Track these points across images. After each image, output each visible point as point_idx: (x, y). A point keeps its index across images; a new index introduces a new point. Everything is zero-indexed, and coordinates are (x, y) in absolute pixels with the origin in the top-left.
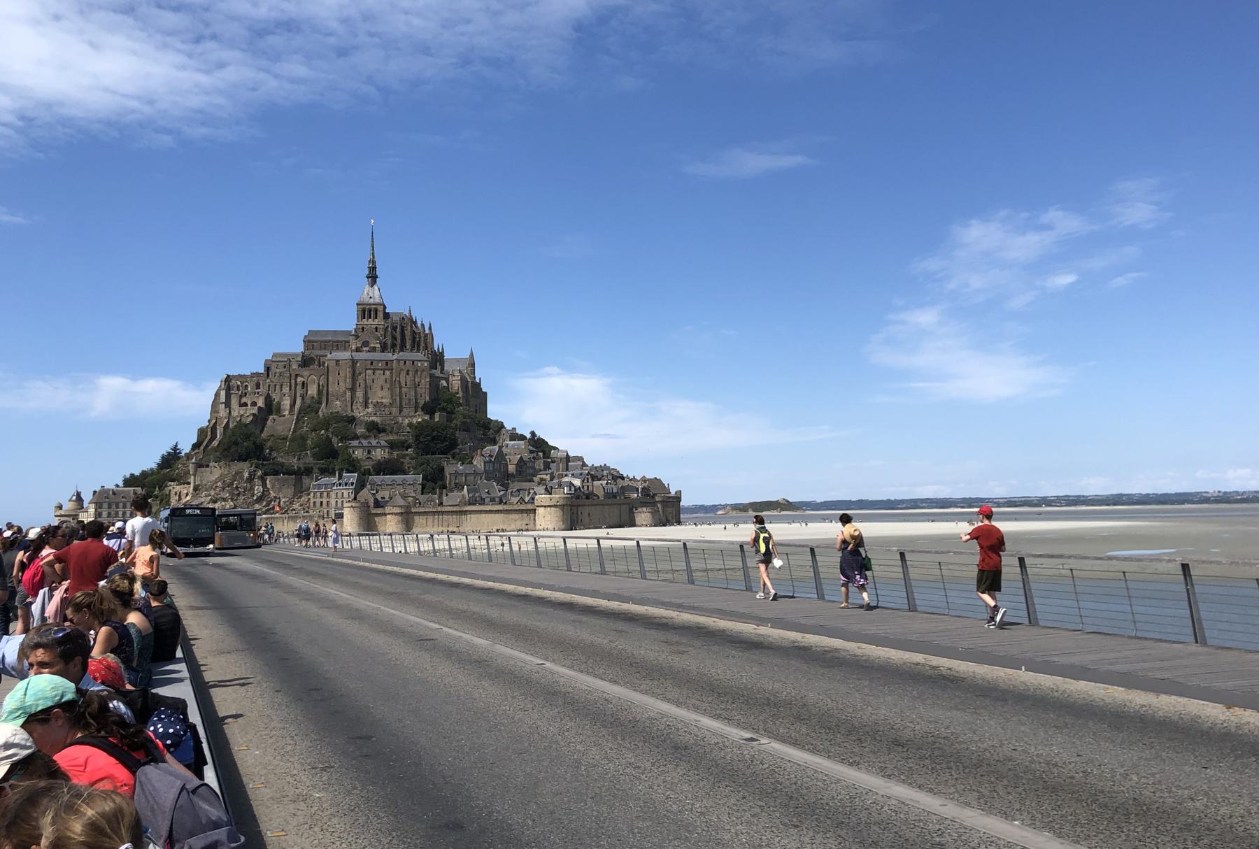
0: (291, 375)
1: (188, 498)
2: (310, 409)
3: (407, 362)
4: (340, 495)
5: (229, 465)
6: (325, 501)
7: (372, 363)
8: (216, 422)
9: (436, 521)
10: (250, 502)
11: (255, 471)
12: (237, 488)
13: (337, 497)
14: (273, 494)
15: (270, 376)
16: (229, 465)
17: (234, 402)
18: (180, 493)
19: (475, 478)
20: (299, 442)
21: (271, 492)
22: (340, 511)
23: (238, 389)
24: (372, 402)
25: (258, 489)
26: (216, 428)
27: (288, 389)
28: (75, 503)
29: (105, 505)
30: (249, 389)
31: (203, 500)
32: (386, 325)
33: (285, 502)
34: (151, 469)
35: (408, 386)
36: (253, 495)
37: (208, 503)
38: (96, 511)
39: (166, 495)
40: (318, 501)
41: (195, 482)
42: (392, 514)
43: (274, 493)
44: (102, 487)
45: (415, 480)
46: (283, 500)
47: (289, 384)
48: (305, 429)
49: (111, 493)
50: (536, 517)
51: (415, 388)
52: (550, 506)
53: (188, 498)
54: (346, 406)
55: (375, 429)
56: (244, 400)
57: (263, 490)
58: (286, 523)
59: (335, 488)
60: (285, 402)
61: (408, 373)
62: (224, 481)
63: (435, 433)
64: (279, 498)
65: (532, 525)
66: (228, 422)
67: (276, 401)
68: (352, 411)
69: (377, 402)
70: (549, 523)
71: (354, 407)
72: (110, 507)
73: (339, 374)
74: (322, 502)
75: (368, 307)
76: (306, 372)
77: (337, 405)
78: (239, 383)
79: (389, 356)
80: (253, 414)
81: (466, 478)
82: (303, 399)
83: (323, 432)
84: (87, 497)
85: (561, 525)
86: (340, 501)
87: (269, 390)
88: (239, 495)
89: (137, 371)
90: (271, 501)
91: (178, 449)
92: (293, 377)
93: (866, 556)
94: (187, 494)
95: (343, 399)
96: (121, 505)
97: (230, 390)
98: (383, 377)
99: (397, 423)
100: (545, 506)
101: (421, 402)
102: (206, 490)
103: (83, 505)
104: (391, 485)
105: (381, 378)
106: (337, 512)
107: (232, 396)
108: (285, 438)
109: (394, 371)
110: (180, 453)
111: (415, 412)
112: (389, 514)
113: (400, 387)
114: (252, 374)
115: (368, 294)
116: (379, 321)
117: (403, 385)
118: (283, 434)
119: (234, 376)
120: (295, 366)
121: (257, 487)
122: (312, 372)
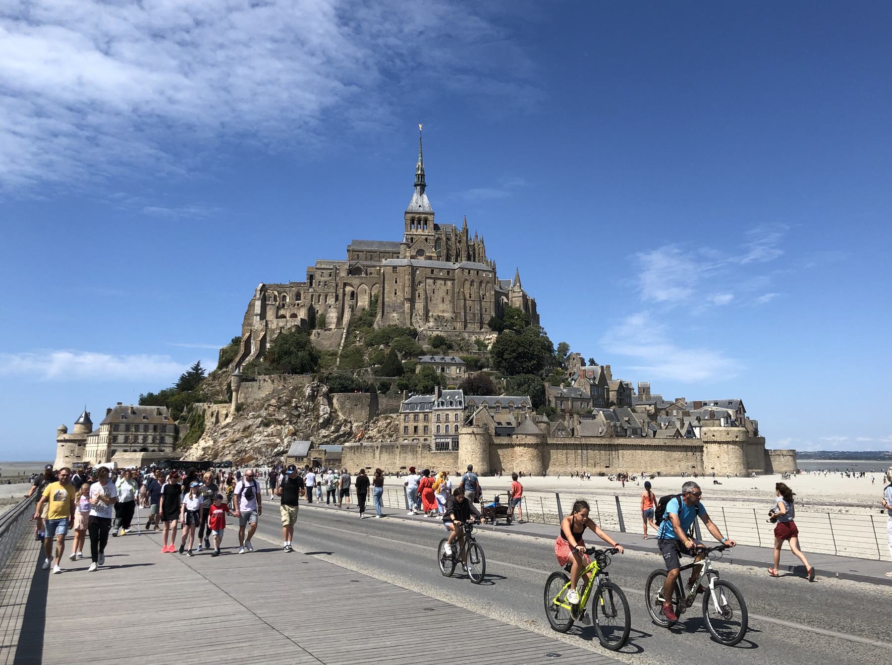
0: (337, 286)
1: (229, 420)
2: (362, 321)
3: (471, 272)
4: (443, 418)
5: (285, 379)
6: (421, 425)
7: (432, 272)
8: (250, 335)
9: (579, 457)
10: (314, 427)
11: (318, 386)
12: (296, 407)
13: (438, 420)
14: (341, 417)
15: (314, 285)
16: (285, 379)
17: (270, 315)
18: (218, 413)
19: (581, 403)
20: (353, 358)
21: (340, 414)
22: (443, 440)
23: (275, 300)
24: (432, 316)
25: (324, 410)
26: (250, 343)
27: (334, 300)
28: (83, 426)
29: (122, 427)
30: (288, 300)
31: (250, 423)
32: (436, 236)
33: (358, 427)
34: (171, 390)
35: (471, 299)
36: (318, 417)
37: (258, 427)
38: (110, 434)
39: (199, 416)
40: (411, 425)
41: (237, 400)
42: (524, 445)
43: (344, 414)
44: (119, 403)
45: (524, 402)
46: (355, 424)
47: (334, 294)
48: (358, 344)
49: (130, 411)
50: (704, 458)
51: (480, 301)
52: (728, 443)
53: (229, 420)
54: (405, 318)
55: (439, 344)
56: (282, 312)
57: (331, 411)
58: (377, 455)
59: (436, 408)
60: (331, 315)
61: (472, 285)
62: (279, 398)
63: (520, 350)
64: (350, 422)
65: (699, 468)
66: (265, 336)
67: (320, 313)
68: (411, 324)
69: (438, 316)
70: (726, 465)
71: (413, 320)
72: (128, 429)
73: (396, 282)
74: (416, 428)
75: (417, 216)
76: (355, 281)
77: (394, 318)
78: (276, 293)
79: (450, 265)
80: (297, 325)
81: (572, 404)
82: (353, 311)
83: (382, 346)
84: (98, 418)
85: (741, 469)
86: (443, 426)
87: (312, 301)
88: (299, 416)
89: (79, 347)
90: (340, 426)
91: (201, 369)
92: (341, 285)
94: (227, 416)
96: (142, 427)
97: (265, 301)
99: (463, 339)
100: (719, 443)
101: (487, 319)
102: (254, 410)
103: (91, 429)
104: (494, 407)
105: (442, 288)
106: (438, 441)
107: (268, 308)
108: (334, 354)
109: (456, 281)
110: (202, 373)
111: (481, 328)
112: (520, 445)
113: (465, 300)
114: (291, 283)
116: (429, 231)
117: (467, 296)
118: (331, 349)
119: (270, 286)
120: (343, 274)
121: (322, 407)
122: (364, 281)
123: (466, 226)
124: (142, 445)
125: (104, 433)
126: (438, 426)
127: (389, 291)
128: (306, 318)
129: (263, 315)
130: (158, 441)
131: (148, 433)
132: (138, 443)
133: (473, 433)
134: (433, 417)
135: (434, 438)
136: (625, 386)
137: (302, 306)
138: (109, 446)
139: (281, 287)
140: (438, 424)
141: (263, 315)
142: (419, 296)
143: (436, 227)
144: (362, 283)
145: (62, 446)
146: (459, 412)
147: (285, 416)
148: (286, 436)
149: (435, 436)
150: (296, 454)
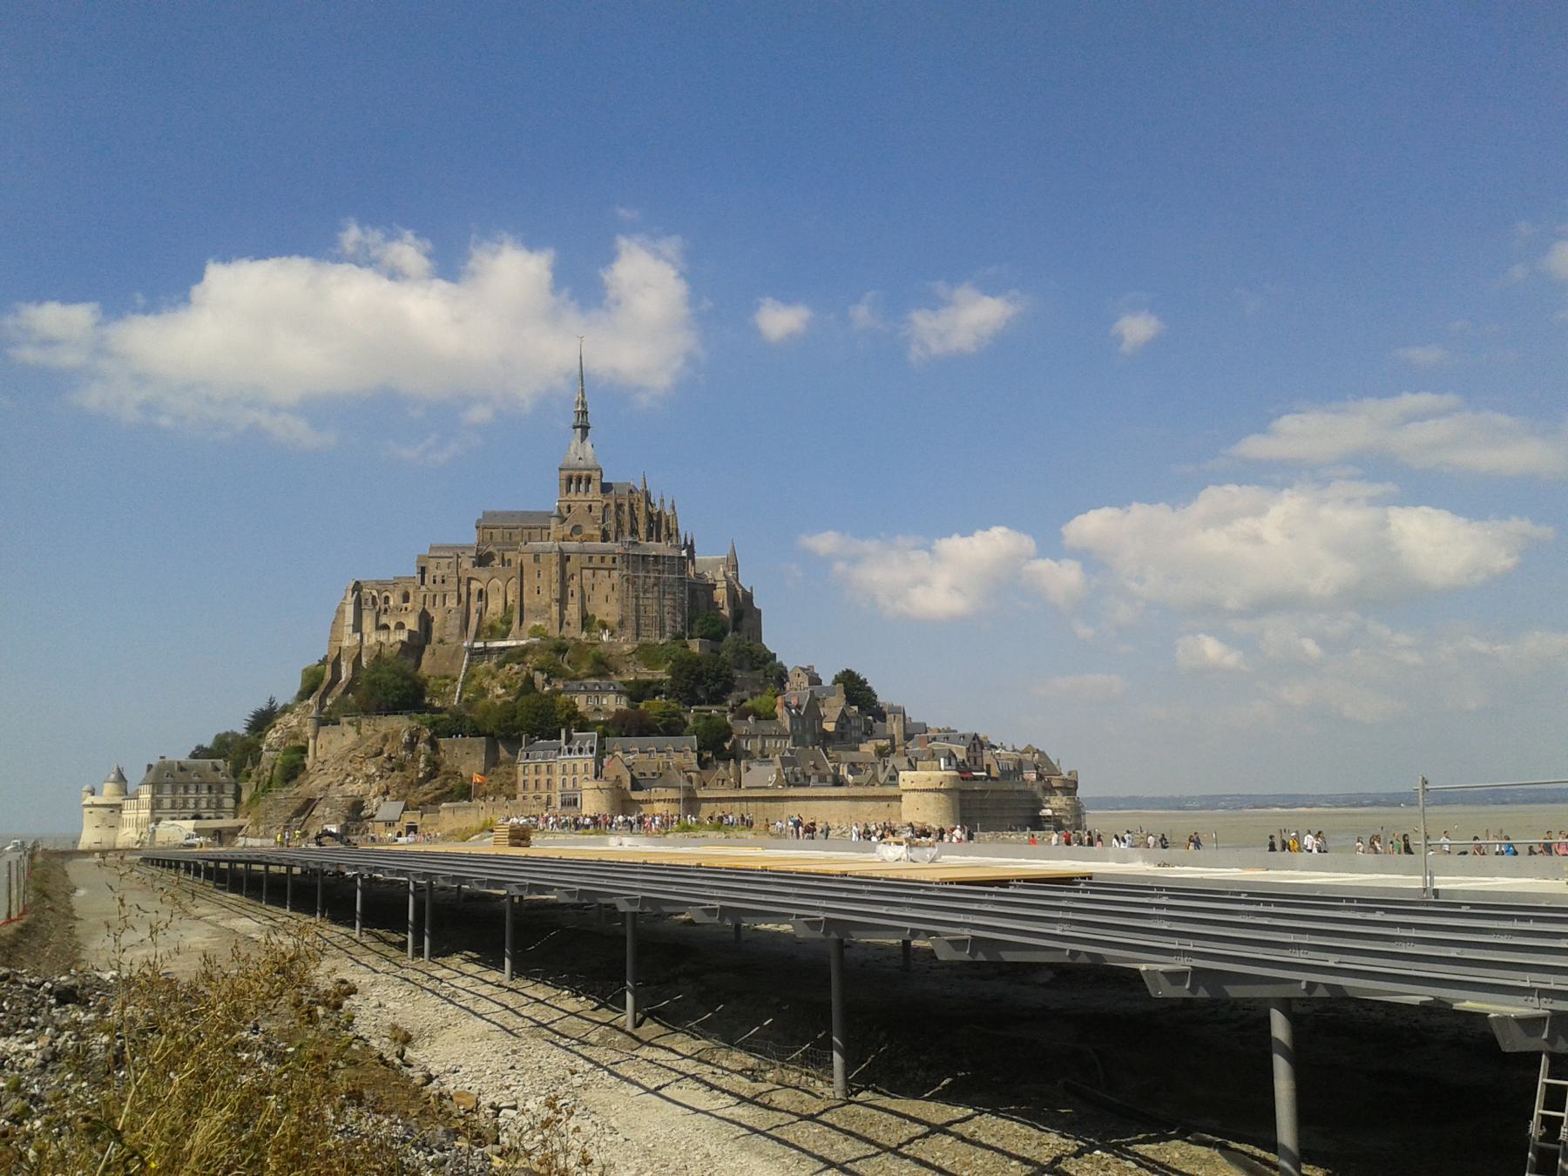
4: (569, 769)
6: (543, 778)
17: (368, 623)
26: (340, 665)
27: (455, 601)
28: (116, 785)
30: (391, 603)
38: (153, 797)
47: (456, 593)
76: (483, 573)
78: (375, 593)
84: (136, 774)
86: (569, 779)
87: (424, 604)
92: (464, 581)
93: (1549, 1010)
95: (547, 616)
98: (608, 582)
115: (576, 454)
123: (646, 487)
124: (194, 811)
125: (146, 796)
126: (564, 779)
127: (529, 589)
128: (416, 629)
129: (357, 627)
130: (214, 806)
131: (201, 796)
132: (189, 808)
133: (598, 788)
134: (558, 768)
135: (559, 794)
136: (138, 846)
137: (411, 611)
138: (152, 813)
139: (382, 585)
140: (563, 777)
141: (357, 627)
142: (572, 595)
143: (606, 488)
144: (493, 578)
145: (91, 812)
146: (588, 762)
147: (374, 770)
148: (375, 797)
149: (561, 791)
150: (385, 818)
